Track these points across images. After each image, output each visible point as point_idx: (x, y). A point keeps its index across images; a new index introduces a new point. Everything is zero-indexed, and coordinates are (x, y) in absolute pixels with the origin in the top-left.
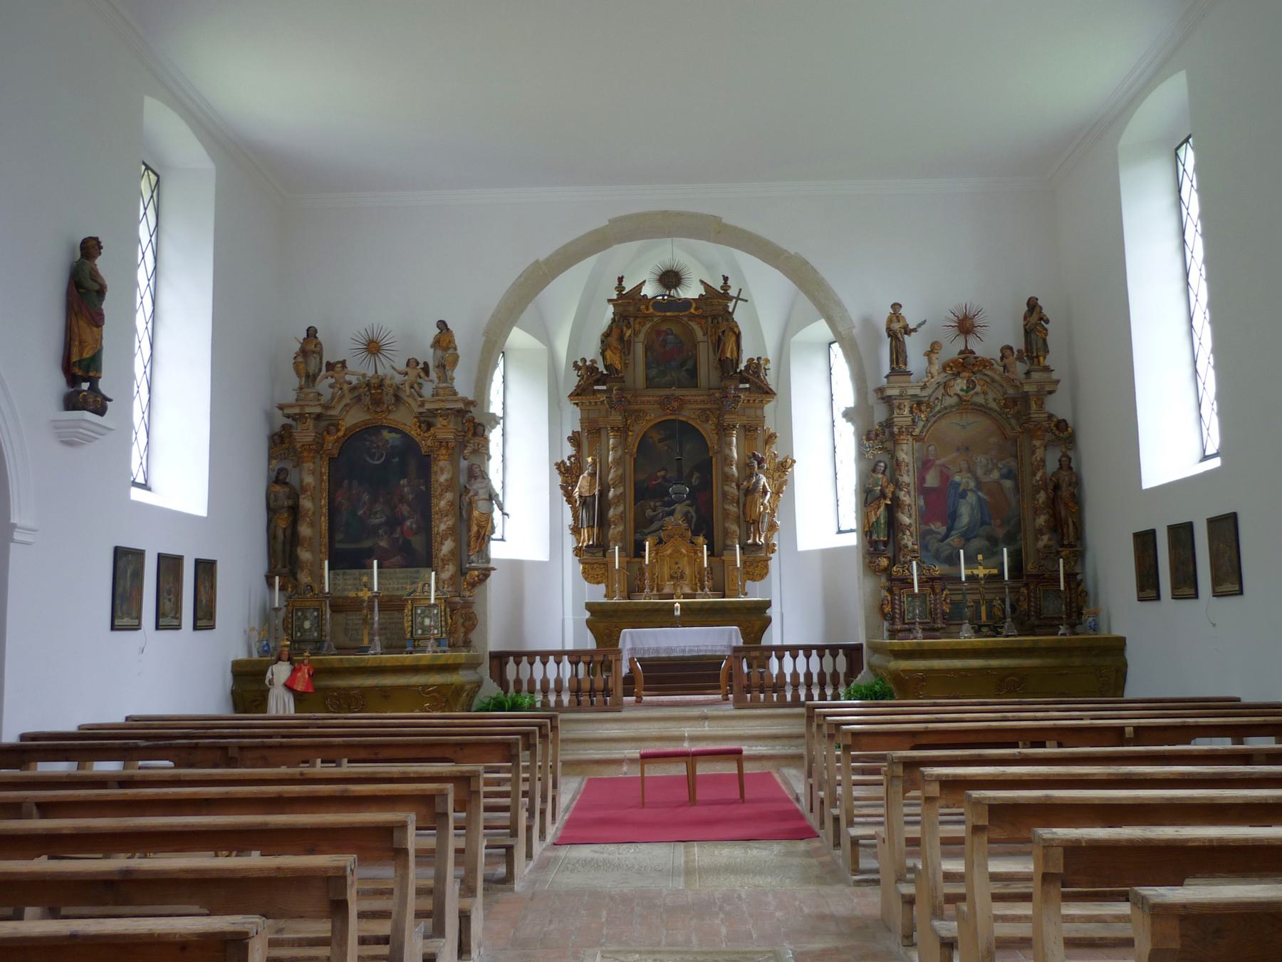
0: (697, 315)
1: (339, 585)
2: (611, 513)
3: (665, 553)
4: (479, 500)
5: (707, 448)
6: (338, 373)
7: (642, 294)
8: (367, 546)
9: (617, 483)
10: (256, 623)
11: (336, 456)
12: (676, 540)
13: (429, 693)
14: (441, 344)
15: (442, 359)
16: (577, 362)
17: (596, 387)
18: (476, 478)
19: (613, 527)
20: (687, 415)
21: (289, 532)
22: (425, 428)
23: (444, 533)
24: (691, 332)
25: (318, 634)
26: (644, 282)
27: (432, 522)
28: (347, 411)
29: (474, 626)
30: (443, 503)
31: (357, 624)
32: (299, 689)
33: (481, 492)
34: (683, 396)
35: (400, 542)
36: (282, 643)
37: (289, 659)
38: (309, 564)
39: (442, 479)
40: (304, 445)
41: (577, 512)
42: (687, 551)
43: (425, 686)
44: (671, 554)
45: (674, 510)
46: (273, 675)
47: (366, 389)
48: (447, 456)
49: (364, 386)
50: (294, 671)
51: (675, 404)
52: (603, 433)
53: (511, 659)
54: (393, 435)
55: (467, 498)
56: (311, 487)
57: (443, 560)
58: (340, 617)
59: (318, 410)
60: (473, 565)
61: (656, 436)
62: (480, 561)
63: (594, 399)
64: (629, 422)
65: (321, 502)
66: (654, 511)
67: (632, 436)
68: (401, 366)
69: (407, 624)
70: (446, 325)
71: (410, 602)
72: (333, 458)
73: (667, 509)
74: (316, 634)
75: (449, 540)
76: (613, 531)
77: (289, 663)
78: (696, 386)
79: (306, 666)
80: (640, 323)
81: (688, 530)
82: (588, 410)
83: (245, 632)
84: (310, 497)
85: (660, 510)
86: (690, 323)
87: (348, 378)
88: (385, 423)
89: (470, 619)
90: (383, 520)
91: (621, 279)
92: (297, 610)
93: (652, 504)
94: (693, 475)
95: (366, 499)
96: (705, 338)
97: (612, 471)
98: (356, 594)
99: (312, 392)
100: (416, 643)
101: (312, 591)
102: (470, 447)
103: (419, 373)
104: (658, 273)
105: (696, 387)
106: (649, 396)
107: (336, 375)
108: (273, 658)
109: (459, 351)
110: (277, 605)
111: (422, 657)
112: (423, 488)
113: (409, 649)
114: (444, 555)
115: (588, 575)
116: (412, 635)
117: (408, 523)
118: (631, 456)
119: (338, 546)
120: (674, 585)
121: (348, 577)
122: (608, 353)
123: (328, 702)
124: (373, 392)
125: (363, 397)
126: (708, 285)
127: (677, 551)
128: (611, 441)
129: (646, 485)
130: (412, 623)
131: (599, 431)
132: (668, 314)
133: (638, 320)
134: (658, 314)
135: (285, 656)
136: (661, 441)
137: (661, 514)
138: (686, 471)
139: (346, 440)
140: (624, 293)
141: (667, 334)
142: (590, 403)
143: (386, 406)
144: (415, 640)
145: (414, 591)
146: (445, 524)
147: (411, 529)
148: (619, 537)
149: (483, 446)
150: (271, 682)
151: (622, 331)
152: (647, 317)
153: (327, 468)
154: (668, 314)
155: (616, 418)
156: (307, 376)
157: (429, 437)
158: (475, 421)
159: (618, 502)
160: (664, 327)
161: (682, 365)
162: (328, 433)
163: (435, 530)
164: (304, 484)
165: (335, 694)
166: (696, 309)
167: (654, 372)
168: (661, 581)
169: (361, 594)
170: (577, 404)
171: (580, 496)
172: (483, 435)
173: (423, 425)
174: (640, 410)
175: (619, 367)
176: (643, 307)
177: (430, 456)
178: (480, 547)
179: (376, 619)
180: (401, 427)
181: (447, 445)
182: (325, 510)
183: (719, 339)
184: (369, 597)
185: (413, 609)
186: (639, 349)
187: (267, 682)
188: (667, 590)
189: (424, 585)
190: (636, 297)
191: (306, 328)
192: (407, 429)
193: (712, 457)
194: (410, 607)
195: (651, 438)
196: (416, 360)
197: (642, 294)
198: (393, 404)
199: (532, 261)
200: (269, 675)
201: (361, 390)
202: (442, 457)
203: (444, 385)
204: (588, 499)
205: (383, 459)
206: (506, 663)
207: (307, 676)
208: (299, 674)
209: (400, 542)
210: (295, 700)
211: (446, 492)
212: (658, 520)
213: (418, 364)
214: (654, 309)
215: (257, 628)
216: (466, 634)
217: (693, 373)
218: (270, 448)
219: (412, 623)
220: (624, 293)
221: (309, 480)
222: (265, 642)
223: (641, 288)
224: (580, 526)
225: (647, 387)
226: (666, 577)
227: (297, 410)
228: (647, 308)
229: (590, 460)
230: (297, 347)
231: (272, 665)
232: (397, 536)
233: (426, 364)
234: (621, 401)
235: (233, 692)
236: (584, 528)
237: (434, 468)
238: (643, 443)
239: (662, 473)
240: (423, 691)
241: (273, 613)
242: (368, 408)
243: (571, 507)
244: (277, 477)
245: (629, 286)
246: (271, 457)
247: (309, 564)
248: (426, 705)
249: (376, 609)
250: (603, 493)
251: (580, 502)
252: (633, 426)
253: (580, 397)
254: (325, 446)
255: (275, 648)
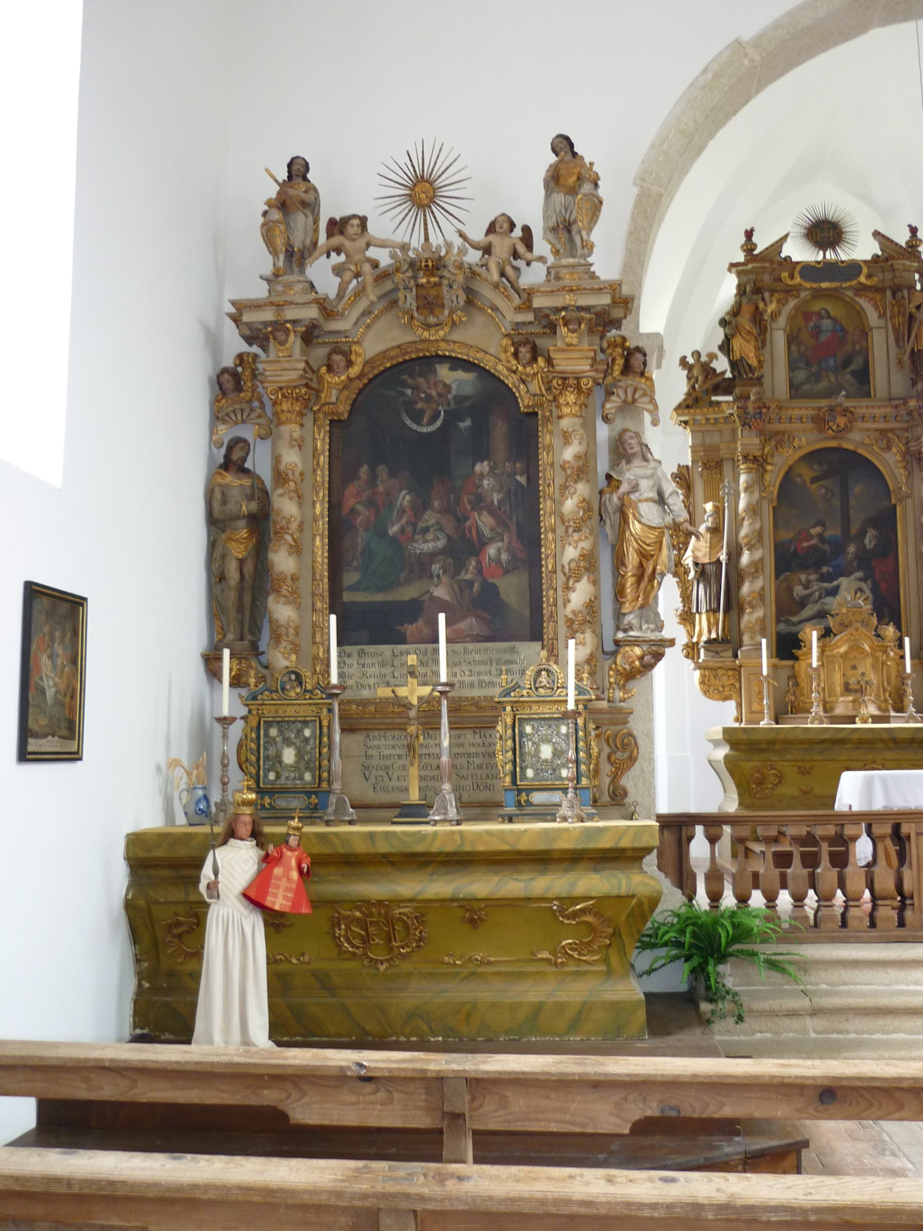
0: (870, 287)
1: (351, 676)
2: (746, 588)
3: (835, 652)
4: (640, 501)
5: (888, 492)
6: (354, 240)
7: (783, 255)
8: (406, 598)
9: (753, 542)
10: (182, 750)
11: (346, 415)
12: (857, 630)
13: (575, 915)
14: (562, 181)
15: (566, 209)
16: (685, 357)
17: (714, 398)
18: (629, 459)
19: (748, 611)
20: (854, 441)
21: (249, 568)
22: (528, 356)
23: (573, 565)
24: (859, 314)
25: (313, 776)
26: (787, 236)
27: (540, 547)
28: (368, 327)
29: (632, 759)
30: (570, 505)
31: (389, 757)
32: (277, 908)
33: (644, 484)
34: (855, 408)
35: (476, 587)
36: (239, 797)
37: (256, 835)
38: (291, 631)
39: (569, 454)
40: (281, 388)
41: (687, 589)
42: (871, 648)
43: (567, 900)
44: (846, 653)
45: (838, 587)
46: (216, 873)
47: (409, 274)
48: (577, 408)
49: (406, 267)
50: (267, 860)
51: (841, 421)
52: (727, 467)
53: (699, 829)
54: (460, 374)
55: (615, 498)
56: (297, 474)
57: (570, 622)
58: (357, 739)
59: (312, 313)
60: (632, 633)
61: (807, 473)
62: (645, 627)
63: (714, 412)
64: (766, 450)
65: (314, 507)
66: (806, 587)
67: (771, 471)
68: (477, 234)
69: (503, 758)
70: (571, 145)
71: (508, 708)
72: (339, 421)
73: (826, 585)
74: (308, 776)
75: (585, 580)
76: (750, 618)
77: (254, 842)
78: (868, 395)
79: (292, 849)
80: (779, 301)
81: (872, 615)
82: (704, 432)
83: (159, 769)
84: (294, 495)
85: (815, 586)
86: (857, 299)
87: (372, 253)
88: (444, 349)
89: (625, 746)
90: (441, 544)
91: (749, 234)
92: (269, 724)
93: (803, 577)
94: (866, 532)
95: (405, 502)
96: (882, 322)
97: (746, 523)
98: (393, 692)
99: (299, 282)
100: (523, 797)
101: (301, 684)
102: (618, 396)
103: (514, 244)
104: (805, 224)
105: (868, 395)
106: (800, 408)
107: (348, 244)
108: (218, 829)
109: (603, 191)
110: (226, 712)
111: (559, 830)
112: (522, 479)
113: (511, 810)
114: (574, 612)
115: (709, 686)
116: (514, 781)
117: (491, 551)
118: (771, 501)
119: (347, 597)
120: (854, 702)
121: (368, 660)
122: (737, 343)
123: (340, 932)
124: (424, 280)
125: (401, 295)
126: (888, 239)
127: (856, 648)
128: (743, 478)
129: (792, 549)
130: (514, 754)
131: (719, 464)
132: (824, 285)
133: (777, 295)
134: (808, 285)
135: (244, 828)
136: (814, 480)
137: (817, 594)
138: (854, 528)
139: (365, 385)
140: (756, 252)
141: (821, 317)
142: (708, 420)
143: (446, 312)
144: (520, 792)
145: (517, 686)
146: (576, 548)
147: (499, 561)
148: (757, 627)
149: (645, 394)
150: (213, 887)
151: (757, 308)
152: (791, 291)
153: (327, 440)
154: (824, 285)
155: (748, 441)
156: (290, 253)
157: (535, 374)
158: (627, 344)
159: (756, 572)
160: (817, 307)
161: (847, 363)
162: (330, 369)
163: (548, 564)
164: (282, 467)
165: (358, 914)
166: (869, 276)
167: (801, 375)
168: (830, 696)
169: (402, 692)
170: (686, 423)
171: (696, 564)
172: (642, 374)
173: (523, 350)
174: (783, 433)
175: (753, 362)
176: (785, 275)
177: (536, 414)
178: (646, 598)
179: (446, 743)
180: (474, 356)
181: (579, 383)
182: (323, 525)
183: (911, 317)
184: (420, 699)
185: (517, 723)
186: (779, 339)
187: (202, 887)
188: (839, 710)
189: (538, 673)
190: (777, 259)
191: (288, 160)
192: (488, 363)
193: (895, 506)
194: (509, 721)
195: (800, 475)
196: (509, 218)
197: (783, 255)
198: (462, 310)
199: (729, 39)
200: (207, 871)
201: (399, 277)
202: (566, 410)
203: (571, 261)
204: (708, 567)
205: (439, 423)
206: (690, 838)
207: (295, 875)
208: (278, 871)
209: (476, 587)
210: (266, 925)
211: (576, 482)
212: (813, 602)
213: (512, 226)
214: (801, 277)
215: (185, 763)
216: (615, 777)
217: (863, 377)
218: (215, 401)
219: (514, 754)
220: (756, 252)
221: (291, 458)
222: (200, 793)
223: (782, 246)
224: (694, 611)
225: (792, 397)
226: (838, 689)
227: (268, 315)
228: (792, 277)
229: (709, 507)
230: (273, 191)
231: (214, 847)
232: (468, 576)
233: (526, 230)
234: (760, 413)
235: (129, 906)
236: (700, 614)
237: (545, 439)
238: (788, 482)
239: (818, 529)
240: (562, 910)
241: (218, 727)
242: (412, 317)
243: (677, 582)
244: (227, 457)
245: (762, 243)
246: (217, 417)
247: (291, 631)
248: (564, 943)
249: (445, 721)
250: (735, 554)
251: (696, 572)
252: (773, 456)
253: (692, 411)
254: (323, 395)
255: (221, 806)
